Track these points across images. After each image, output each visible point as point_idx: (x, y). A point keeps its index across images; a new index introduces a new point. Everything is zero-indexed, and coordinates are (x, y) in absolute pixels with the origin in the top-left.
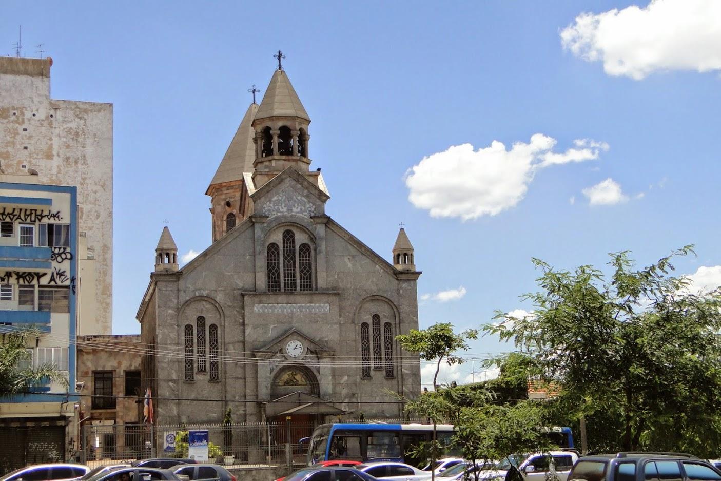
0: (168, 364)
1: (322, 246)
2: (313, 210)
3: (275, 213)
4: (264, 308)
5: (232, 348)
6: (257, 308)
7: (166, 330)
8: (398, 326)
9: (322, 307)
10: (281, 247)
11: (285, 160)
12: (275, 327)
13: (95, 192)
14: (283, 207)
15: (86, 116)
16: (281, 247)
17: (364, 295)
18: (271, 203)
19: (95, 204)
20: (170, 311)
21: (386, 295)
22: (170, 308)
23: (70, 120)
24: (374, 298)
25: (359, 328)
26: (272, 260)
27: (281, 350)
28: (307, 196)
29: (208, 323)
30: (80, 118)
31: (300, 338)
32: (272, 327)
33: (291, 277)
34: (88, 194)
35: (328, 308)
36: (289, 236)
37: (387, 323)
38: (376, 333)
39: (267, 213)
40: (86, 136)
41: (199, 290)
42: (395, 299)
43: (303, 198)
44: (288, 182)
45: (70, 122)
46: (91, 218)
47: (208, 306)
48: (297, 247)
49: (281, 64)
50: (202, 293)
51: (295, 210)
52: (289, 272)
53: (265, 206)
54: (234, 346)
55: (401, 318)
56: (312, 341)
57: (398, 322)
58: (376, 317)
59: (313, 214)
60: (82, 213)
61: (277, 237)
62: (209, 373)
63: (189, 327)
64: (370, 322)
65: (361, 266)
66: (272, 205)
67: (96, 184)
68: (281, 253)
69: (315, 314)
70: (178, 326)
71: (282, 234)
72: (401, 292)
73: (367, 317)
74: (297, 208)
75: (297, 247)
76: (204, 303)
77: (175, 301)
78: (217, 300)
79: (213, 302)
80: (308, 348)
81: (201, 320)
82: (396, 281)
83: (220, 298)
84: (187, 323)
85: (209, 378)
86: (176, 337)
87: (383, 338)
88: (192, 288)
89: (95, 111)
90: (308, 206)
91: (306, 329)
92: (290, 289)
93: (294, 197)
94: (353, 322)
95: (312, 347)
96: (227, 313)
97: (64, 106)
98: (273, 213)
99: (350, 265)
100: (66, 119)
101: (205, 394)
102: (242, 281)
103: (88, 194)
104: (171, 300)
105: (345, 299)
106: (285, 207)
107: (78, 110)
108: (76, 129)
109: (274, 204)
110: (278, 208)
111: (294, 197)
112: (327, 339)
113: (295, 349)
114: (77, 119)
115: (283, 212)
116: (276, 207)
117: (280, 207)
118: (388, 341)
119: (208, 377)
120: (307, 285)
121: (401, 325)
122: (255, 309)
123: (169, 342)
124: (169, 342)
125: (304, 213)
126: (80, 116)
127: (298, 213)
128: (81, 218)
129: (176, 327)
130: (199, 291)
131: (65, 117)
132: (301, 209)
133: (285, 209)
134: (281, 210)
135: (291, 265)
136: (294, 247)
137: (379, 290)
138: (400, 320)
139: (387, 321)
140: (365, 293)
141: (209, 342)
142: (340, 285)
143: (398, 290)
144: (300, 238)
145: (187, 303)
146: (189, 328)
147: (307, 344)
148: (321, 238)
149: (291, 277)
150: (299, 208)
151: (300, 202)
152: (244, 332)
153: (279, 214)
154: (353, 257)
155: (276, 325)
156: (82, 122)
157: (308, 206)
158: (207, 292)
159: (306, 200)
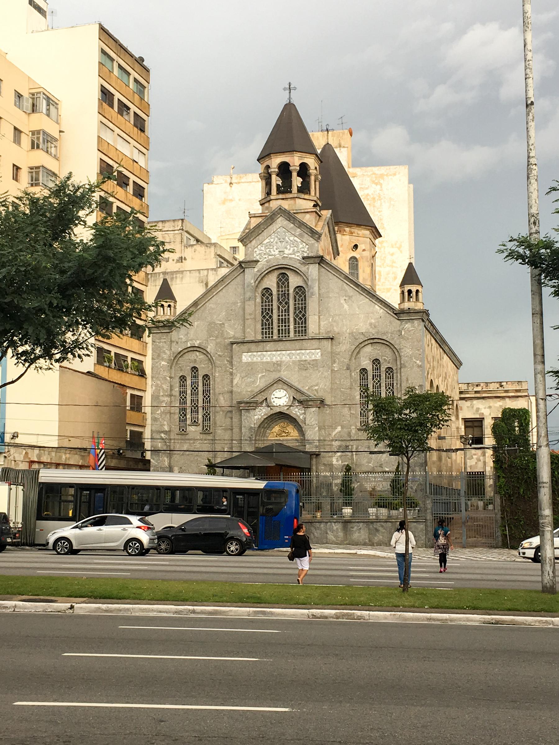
0: (161, 416)
1: (315, 288)
2: (306, 250)
3: (266, 256)
4: (301, 355)
5: (222, 398)
6: (246, 358)
7: (159, 382)
8: (399, 371)
9: (313, 354)
10: (275, 292)
11: (283, 199)
12: (264, 376)
13: (392, 254)
14: (275, 249)
15: (381, 181)
16: (275, 292)
17: (362, 339)
18: (262, 246)
19: (392, 266)
20: (163, 363)
21: (384, 338)
22: (163, 359)
23: (367, 187)
24: (374, 341)
25: (356, 375)
26: (266, 305)
27: (266, 399)
28: (300, 236)
29: (201, 373)
30: (376, 184)
31: (285, 387)
32: (260, 376)
33: (285, 323)
34: (385, 257)
35: (320, 354)
36: (283, 279)
37: (389, 368)
38: (377, 379)
39: (258, 257)
40: (382, 201)
41: (191, 340)
42: (395, 341)
43: (296, 238)
44: (281, 221)
45: (367, 188)
46: (389, 281)
47: (202, 357)
48: (291, 291)
49: (291, 97)
50: (194, 344)
51: (287, 252)
52: (284, 317)
53: (256, 250)
54: (223, 396)
55: (402, 362)
56: (298, 390)
57: (399, 367)
58: (376, 362)
59: (305, 255)
60: (380, 275)
61: (271, 282)
62: (201, 424)
63: (183, 378)
64: (369, 368)
65: (359, 308)
66: (263, 248)
67: (393, 247)
68: (275, 298)
69: (306, 360)
70: (170, 377)
71: (276, 278)
72: (403, 333)
73: (366, 362)
74: (289, 250)
75: (291, 291)
76: (198, 353)
77: (168, 352)
78: (208, 350)
79: (205, 352)
80: (294, 398)
81: (195, 369)
82: (398, 321)
83: (210, 348)
84: (181, 374)
85: (201, 429)
86: (169, 388)
87: (383, 385)
88: (184, 339)
89: (390, 175)
90: (301, 246)
91: (294, 379)
92: (283, 337)
93: (287, 238)
94: (348, 369)
95: (299, 397)
96: (218, 362)
97: (362, 173)
98: (265, 256)
99: (346, 306)
100: (362, 186)
101: (198, 446)
102: (232, 332)
103: (385, 257)
104: (164, 352)
105: (339, 344)
106: (277, 249)
107: (374, 176)
108: (372, 194)
109: (265, 247)
110: (270, 251)
111: (287, 238)
112: (316, 388)
113: (280, 399)
114: (374, 185)
115: (275, 255)
116: (268, 250)
117: (271, 250)
118: (389, 388)
119: (200, 428)
120: (302, 330)
121: (402, 370)
122: (243, 357)
123: (162, 394)
124: (162, 394)
125: (297, 255)
126: (376, 181)
127: (291, 254)
128: (379, 280)
129: (168, 378)
130: (191, 342)
131: (362, 184)
132: (294, 250)
133: (277, 252)
134: (273, 253)
135: (285, 310)
136: (288, 291)
137: (377, 333)
138: (401, 364)
139: (389, 366)
140: (362, 336)
141: (202, 393)
142: (335, 328)
143: (400, 331)
144: (294, 281)
145: (181, 354)
146: (183, 378)
147: (293, 393)
148: (313, 280)
149: (285, 323)
150: (292, 249)
151: (293, 243)
152: (232, 382)
153: (270, 257)
154: (350, 297)
155: (264, 374)
156: (379, 187)
157: (301, 246)
158: (198, 342)
159: (299, 241)
